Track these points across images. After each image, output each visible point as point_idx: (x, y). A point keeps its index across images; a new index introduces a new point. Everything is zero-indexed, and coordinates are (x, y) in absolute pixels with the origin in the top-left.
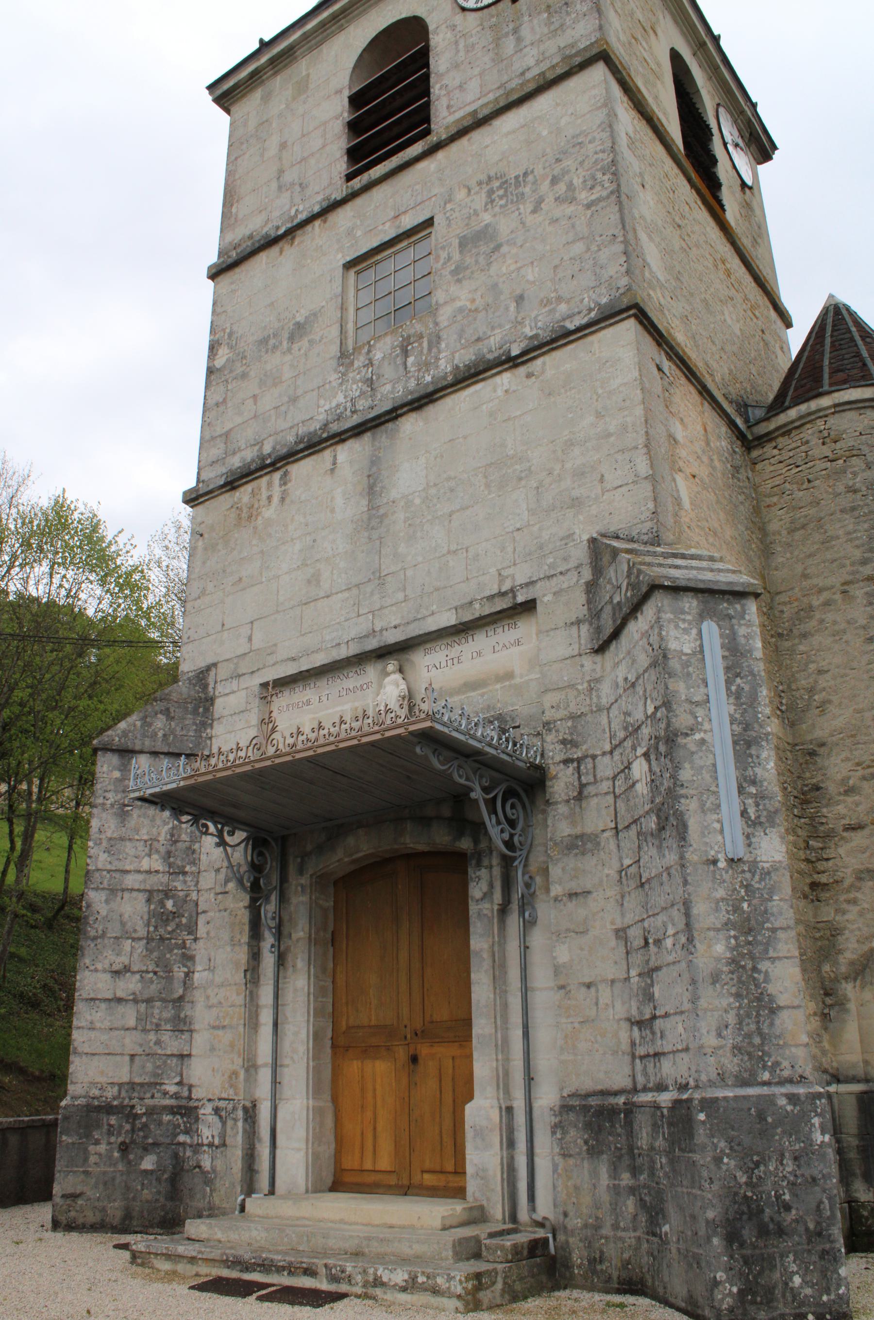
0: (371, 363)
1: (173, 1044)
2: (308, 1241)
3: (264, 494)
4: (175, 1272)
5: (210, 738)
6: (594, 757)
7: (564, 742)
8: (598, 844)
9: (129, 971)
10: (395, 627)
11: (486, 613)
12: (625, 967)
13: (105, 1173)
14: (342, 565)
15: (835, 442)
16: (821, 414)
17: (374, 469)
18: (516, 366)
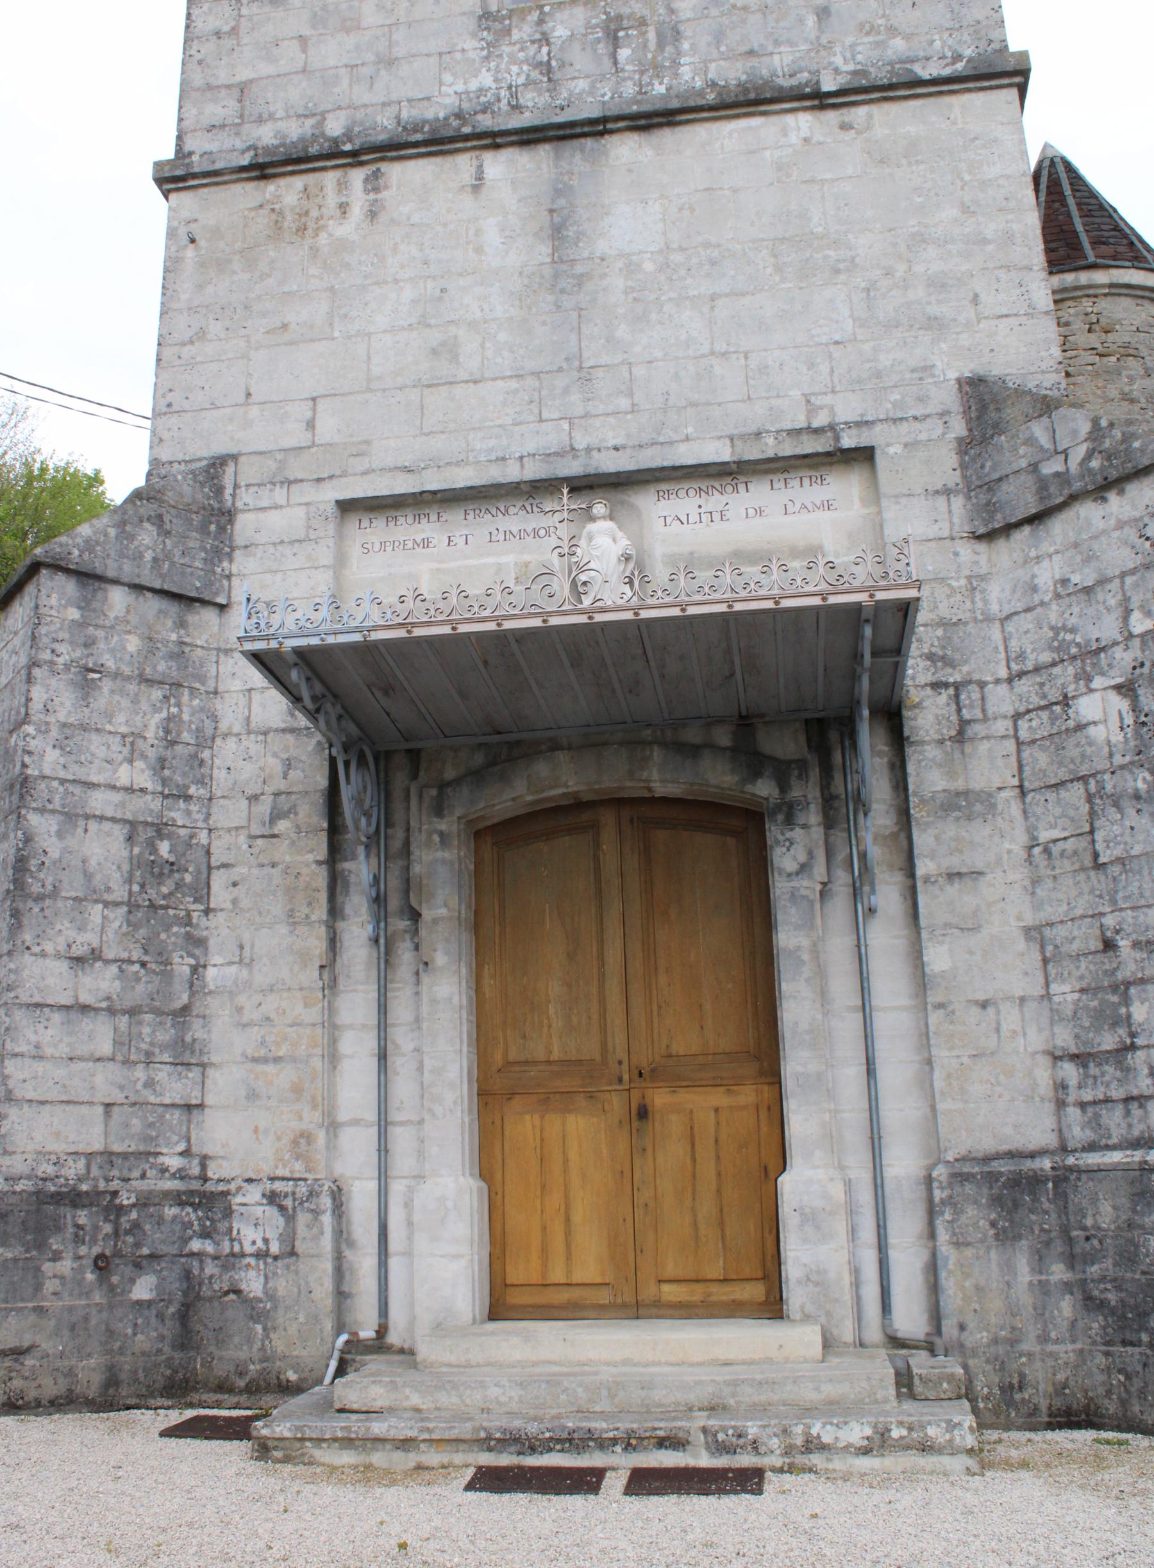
0: (545, 39)
1: (175, 1087)
2: (612, 1396)
3: (332, 199)
4: (369, 1467)
5: (229, 577)
6: (982, 685)
7: (931, 657)
8: (993, 806)
9: (100, 958)
10: (616, 449)
11: (788, 453)
12: (1042, 980)
13: (71, 1309)
14: (502, 337)
15: (1106, 332)
16: (1091, 292)
17: (562, 202)
18: (822, 107)
